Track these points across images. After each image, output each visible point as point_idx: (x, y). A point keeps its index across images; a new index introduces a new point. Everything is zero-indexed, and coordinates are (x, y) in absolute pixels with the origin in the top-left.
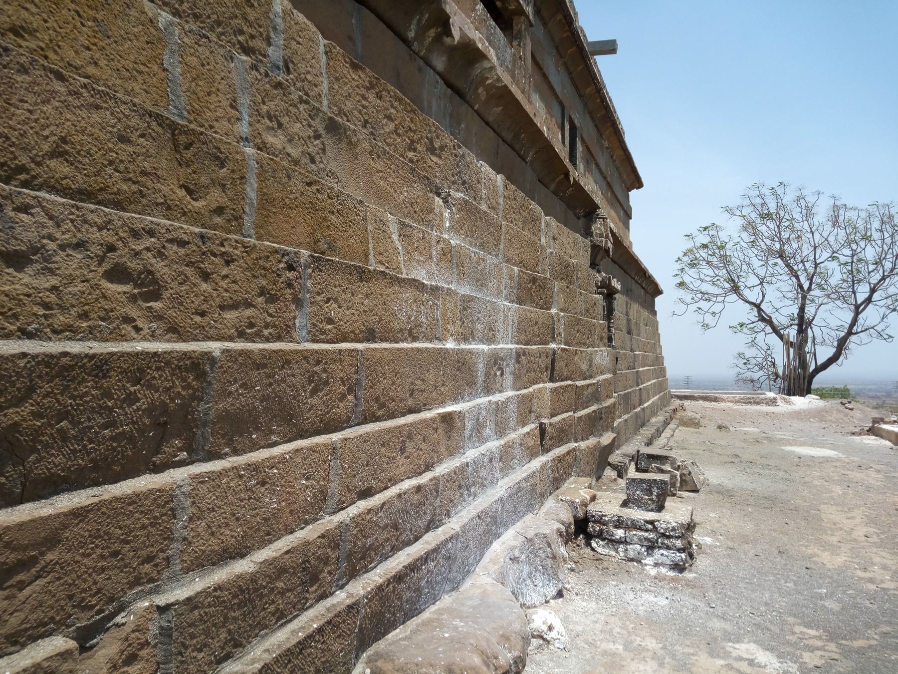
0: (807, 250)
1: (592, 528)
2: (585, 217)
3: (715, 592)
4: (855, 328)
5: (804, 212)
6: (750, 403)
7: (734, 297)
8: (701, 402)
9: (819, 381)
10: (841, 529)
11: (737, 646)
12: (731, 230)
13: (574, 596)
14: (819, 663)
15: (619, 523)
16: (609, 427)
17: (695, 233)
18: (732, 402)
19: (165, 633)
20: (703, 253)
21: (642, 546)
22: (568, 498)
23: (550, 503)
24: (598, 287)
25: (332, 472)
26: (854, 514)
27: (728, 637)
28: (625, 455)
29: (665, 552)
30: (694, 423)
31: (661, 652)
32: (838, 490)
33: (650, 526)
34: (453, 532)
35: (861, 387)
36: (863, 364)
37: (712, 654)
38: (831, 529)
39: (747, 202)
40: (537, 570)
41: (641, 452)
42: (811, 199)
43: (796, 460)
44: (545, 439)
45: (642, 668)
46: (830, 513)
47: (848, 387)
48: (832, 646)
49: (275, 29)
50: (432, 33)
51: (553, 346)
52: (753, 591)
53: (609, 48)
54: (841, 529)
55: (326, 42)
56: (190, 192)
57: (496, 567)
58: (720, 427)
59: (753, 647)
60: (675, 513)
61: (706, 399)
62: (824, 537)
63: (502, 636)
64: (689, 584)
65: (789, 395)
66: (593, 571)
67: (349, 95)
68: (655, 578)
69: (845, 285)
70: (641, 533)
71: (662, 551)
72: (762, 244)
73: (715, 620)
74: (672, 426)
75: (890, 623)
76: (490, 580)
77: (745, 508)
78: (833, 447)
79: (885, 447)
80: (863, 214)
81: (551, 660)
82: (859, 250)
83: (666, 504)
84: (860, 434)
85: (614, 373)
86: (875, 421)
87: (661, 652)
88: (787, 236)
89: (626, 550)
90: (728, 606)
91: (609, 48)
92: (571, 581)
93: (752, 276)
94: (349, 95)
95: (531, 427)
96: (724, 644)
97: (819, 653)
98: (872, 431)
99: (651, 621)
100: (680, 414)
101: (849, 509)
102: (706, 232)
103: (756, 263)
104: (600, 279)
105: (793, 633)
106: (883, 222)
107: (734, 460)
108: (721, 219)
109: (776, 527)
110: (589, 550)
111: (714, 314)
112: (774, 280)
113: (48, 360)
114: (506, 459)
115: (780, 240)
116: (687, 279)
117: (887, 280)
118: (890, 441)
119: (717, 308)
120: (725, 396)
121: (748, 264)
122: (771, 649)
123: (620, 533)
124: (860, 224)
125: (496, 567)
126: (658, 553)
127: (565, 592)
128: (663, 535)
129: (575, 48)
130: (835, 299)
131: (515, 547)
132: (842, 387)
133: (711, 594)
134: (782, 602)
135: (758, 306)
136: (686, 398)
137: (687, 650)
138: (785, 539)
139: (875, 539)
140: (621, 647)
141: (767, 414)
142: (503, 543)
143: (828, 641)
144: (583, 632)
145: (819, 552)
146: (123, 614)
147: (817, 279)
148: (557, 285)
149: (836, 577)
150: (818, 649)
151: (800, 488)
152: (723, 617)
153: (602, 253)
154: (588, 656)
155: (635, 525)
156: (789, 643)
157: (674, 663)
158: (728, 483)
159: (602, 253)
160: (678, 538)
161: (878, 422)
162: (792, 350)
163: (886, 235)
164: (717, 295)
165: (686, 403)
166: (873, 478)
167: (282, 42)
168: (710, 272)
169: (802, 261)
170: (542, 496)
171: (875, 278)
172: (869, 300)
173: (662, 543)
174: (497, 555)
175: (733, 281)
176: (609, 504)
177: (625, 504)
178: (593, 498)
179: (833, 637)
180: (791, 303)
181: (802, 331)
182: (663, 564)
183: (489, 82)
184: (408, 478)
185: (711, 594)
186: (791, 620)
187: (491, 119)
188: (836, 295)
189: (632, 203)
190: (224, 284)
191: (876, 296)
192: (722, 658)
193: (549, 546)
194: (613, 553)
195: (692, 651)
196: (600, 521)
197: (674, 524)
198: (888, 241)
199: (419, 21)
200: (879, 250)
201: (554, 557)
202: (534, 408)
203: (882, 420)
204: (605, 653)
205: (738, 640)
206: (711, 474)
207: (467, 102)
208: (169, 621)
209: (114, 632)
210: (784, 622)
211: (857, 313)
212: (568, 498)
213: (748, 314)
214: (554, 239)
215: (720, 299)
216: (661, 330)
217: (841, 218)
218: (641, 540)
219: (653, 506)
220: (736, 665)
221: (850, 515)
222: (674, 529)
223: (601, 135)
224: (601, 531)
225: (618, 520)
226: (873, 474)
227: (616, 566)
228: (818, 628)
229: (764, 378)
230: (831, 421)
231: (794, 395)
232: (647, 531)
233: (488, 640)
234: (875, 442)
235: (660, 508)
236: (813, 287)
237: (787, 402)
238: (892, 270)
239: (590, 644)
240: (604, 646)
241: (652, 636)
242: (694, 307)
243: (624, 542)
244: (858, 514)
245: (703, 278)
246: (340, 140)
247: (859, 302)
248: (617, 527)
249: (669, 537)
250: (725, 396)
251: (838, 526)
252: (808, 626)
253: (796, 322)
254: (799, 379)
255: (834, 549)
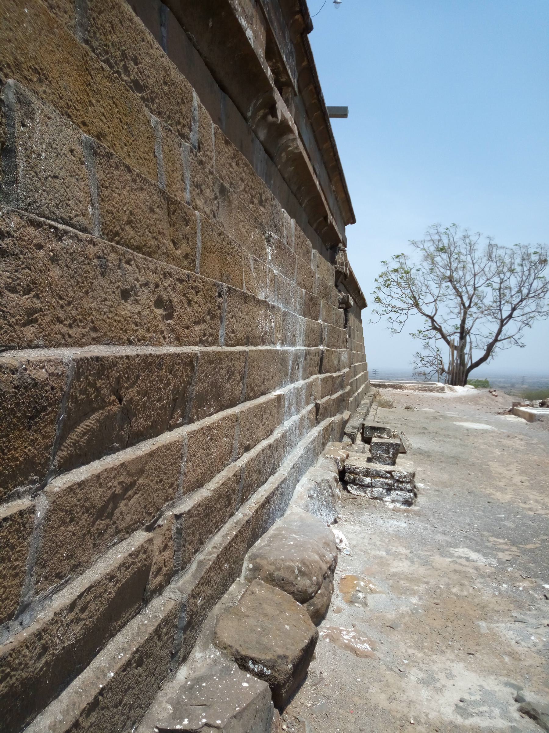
0: (469, 277)
1: (347, 476)
2: (331, 248)
3: (434, 518)
4: (500, 336)
5: (468, 248)
6: (426, 390)
7: (415, 310)
8: (390, 389)
9: (474, 374)
10: (504, 477)
11: (456, 550)
12: (415, 259)
13: (344, 523)
14: (509, 558)
15: (367, 473)
16: (346, 408)
17: (389, 260)
18: (413, 389)
19: (179, 531)
20: (394, 276)
21: (383, 488)
22: (332, 456)
23: (321, 460)
24: (340, 303)
25: (236, 433)
26: (511, 468)
27: (449, 545)
28: (354, 428)
29: (399, 493)
30: (388, 405)
31: (410, 555)
32: (497, 452)
33: (389, 475)
34: (284, 477)
35: (494, 380)
36: (506, 363)
37: (442, 555)
38: (498, 477)
39: (428, 238)
40: (323, 504)
41: (366, 425)
42: (473, 238)
43: (465, 431)
44: (319, 413)
45: (401, 565)
46: (495, 467)
47: (488, 379)
48: (514, 549)
49: (194, 119)
50: (261, 113)
51: (321, 347)
52: (459, 517)
53: (342, 113)
54: (504, 477)
55: (215, 125)
56: (175, 244)
57: (303, 501)
58: (407, 408)
59: (466, 550)
60: (403, 466)
61: (394, 387)
62: (495, 483)
63: (325, 543)
64: (416, 513)
65: (452, 384)
66: (351, 506)
67: (224, 165)
68: (393, 510)
69: (495, 305)
70: (382, 480)
71: (397, 492)
72: (437, 270)
73: (439, 535)
74: (374, 406)
75: (546, 534)
76: (300, 510)
77: (440, 464)
78: (488, 423)
79: (522, 423)
80: (509, 252)
81: (343, 562)
82: (505, 279)
83: (397, 460)
84: (504, 414)
85: (350, 367)
86: (515, 404)
87: (410, 555)
88: (455, 265)
89: (372, 491)
90: (445, 526)
91: (342, 113)
92: (342, 514)
93: (429, 295)
94: (224, 165)
95: (311, 406)
96: (448, 549)
97: (507, 553)
98: (512, 412)
99: (398, 536)
100: (378, 398)
101: (507, 464)
102: (397, 260)
103: (433, 286)
104: (341, 297)
105: (489, 542)
106: (523, 260)
107: (424, 431)
108: (408, 250)
109: (463, 476)
110: (346, 492)
111: (400, 322)
112: (445, 299)
113: (145, 358)
114: (300, 427)
115: (451, 269)
116: (381, 295)
117: (524, 302)
118: (525, 418)
119: (403, 318)
120: (407, 385)
121: (428, 287)
122: (478, 551)
123: (368, 480)
124: (507, 260)
125: (303, 501)
126: (394, 493)
127: (338, 520)
128: (398, 481)
129: (319, 112)
130: (488, 315)
131: (311, 488)
132: (484, 379)
133: (431, 519)
134: (477, 524)
135: (432, 318)
136: (380, 386)
137: (426, 553)
138: (471, 484)
139: (527, 484)
140: (384, 553)
141: (439, 398)
142: (302, 486)
143: (511, 545)
144: (357, 544)
145: (494, 492)
146: (161, 519)
147: (475, 299)
148: (322, 302)
149: (508, 507)
150: (507, 550)
151: (473, 450)
152: (444, 533)
153: (342, 276)
154: (365, 559)
155: (378, 475)
156: (487, 547)
157: (420, 561)
158: (425, 448)
159: (342, 276)
160: (408, 483)
161: (517, 406)
162: (455, 352)
163: (525, 269)
164: (403, 309)
165: (381, 390)
166: (518, 444)
167: (197, 129)
168: (398, 291)
169: (465, 285)
170: (318, 455)
171: (515, 300)
172: (510, 317)
173: (397, 487)
174: (301, 494)
175: (415, 298)
176: (358, 460)
177: (369, 460)
178: (348, 456)
179: (514, 543)
180: (455, 316)
181: (462, 337)
182: (397, 501)
183: (290, 149)
184: (264, 439)
185: (431, 519)
186: (486, 533)
187: (286, 176)
188: (488, 311)
189: (347, 234)
190: (196, 306)
191: (515, 313)
192: (449, 557)
193: (331, 488)
194: (363, 494)
195: (429, 554)
196: (354, 472)
197: (406, 474)
198: (526, 273)
199: (255, 104)
200: (519, 279)
201: (333, 496)
202: (313, 393)
203: (519, 404)
204: (375, 557)
205: (456, 546)
206: (413, 442)
207: (274, 163)
208: (181, 525)
209: (158, 530)
210: (482, 535)
211: (502, 325)
212: (332, 456)
213: (423, 323)
214: (318, 267)
215: (405, 312)
216: (364, 335)
217: (494, 254)
218: (383, 485)
219: (389, 462)
220: (459, 561)
221: (508, 469)
222: (405, 477)
223: (330, 180)
224: (355, 479)
225: (367, 471)
226: (518, 442)
227: (366, 502)
228: (503, 538)
229: (434, 372)
230: (482, 404)
231: (455, 385)
232: (386, 478)
233: (318, 546)
234: (514, 420)
235: (394, 463)
236: (472, 305)
237: (452, 390)
238: (527, 295)
239: (364, 552)
240: (373, 553)
241: (402, 546)
242: (387, 316)
243: (371, 486)
244: (513, 467)
245: (395, 296)
246: (225, 199)
247: (504, 318)
248: (366, 476)
249: (402, 482)
250: (407, 385)
251: (502, 475)
252: (497, 537)
253: (459, 331)
254: (459, 374)
255: (502, 490)
